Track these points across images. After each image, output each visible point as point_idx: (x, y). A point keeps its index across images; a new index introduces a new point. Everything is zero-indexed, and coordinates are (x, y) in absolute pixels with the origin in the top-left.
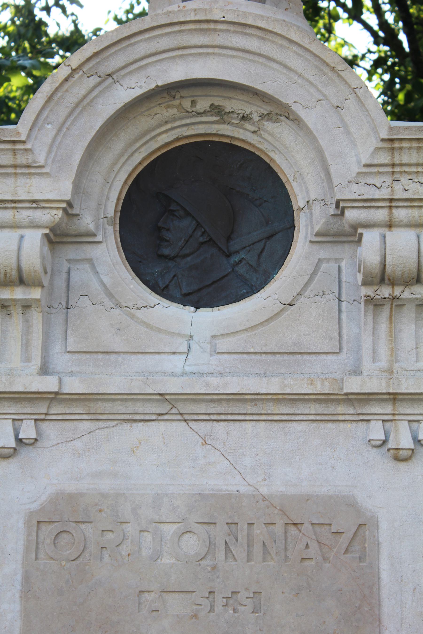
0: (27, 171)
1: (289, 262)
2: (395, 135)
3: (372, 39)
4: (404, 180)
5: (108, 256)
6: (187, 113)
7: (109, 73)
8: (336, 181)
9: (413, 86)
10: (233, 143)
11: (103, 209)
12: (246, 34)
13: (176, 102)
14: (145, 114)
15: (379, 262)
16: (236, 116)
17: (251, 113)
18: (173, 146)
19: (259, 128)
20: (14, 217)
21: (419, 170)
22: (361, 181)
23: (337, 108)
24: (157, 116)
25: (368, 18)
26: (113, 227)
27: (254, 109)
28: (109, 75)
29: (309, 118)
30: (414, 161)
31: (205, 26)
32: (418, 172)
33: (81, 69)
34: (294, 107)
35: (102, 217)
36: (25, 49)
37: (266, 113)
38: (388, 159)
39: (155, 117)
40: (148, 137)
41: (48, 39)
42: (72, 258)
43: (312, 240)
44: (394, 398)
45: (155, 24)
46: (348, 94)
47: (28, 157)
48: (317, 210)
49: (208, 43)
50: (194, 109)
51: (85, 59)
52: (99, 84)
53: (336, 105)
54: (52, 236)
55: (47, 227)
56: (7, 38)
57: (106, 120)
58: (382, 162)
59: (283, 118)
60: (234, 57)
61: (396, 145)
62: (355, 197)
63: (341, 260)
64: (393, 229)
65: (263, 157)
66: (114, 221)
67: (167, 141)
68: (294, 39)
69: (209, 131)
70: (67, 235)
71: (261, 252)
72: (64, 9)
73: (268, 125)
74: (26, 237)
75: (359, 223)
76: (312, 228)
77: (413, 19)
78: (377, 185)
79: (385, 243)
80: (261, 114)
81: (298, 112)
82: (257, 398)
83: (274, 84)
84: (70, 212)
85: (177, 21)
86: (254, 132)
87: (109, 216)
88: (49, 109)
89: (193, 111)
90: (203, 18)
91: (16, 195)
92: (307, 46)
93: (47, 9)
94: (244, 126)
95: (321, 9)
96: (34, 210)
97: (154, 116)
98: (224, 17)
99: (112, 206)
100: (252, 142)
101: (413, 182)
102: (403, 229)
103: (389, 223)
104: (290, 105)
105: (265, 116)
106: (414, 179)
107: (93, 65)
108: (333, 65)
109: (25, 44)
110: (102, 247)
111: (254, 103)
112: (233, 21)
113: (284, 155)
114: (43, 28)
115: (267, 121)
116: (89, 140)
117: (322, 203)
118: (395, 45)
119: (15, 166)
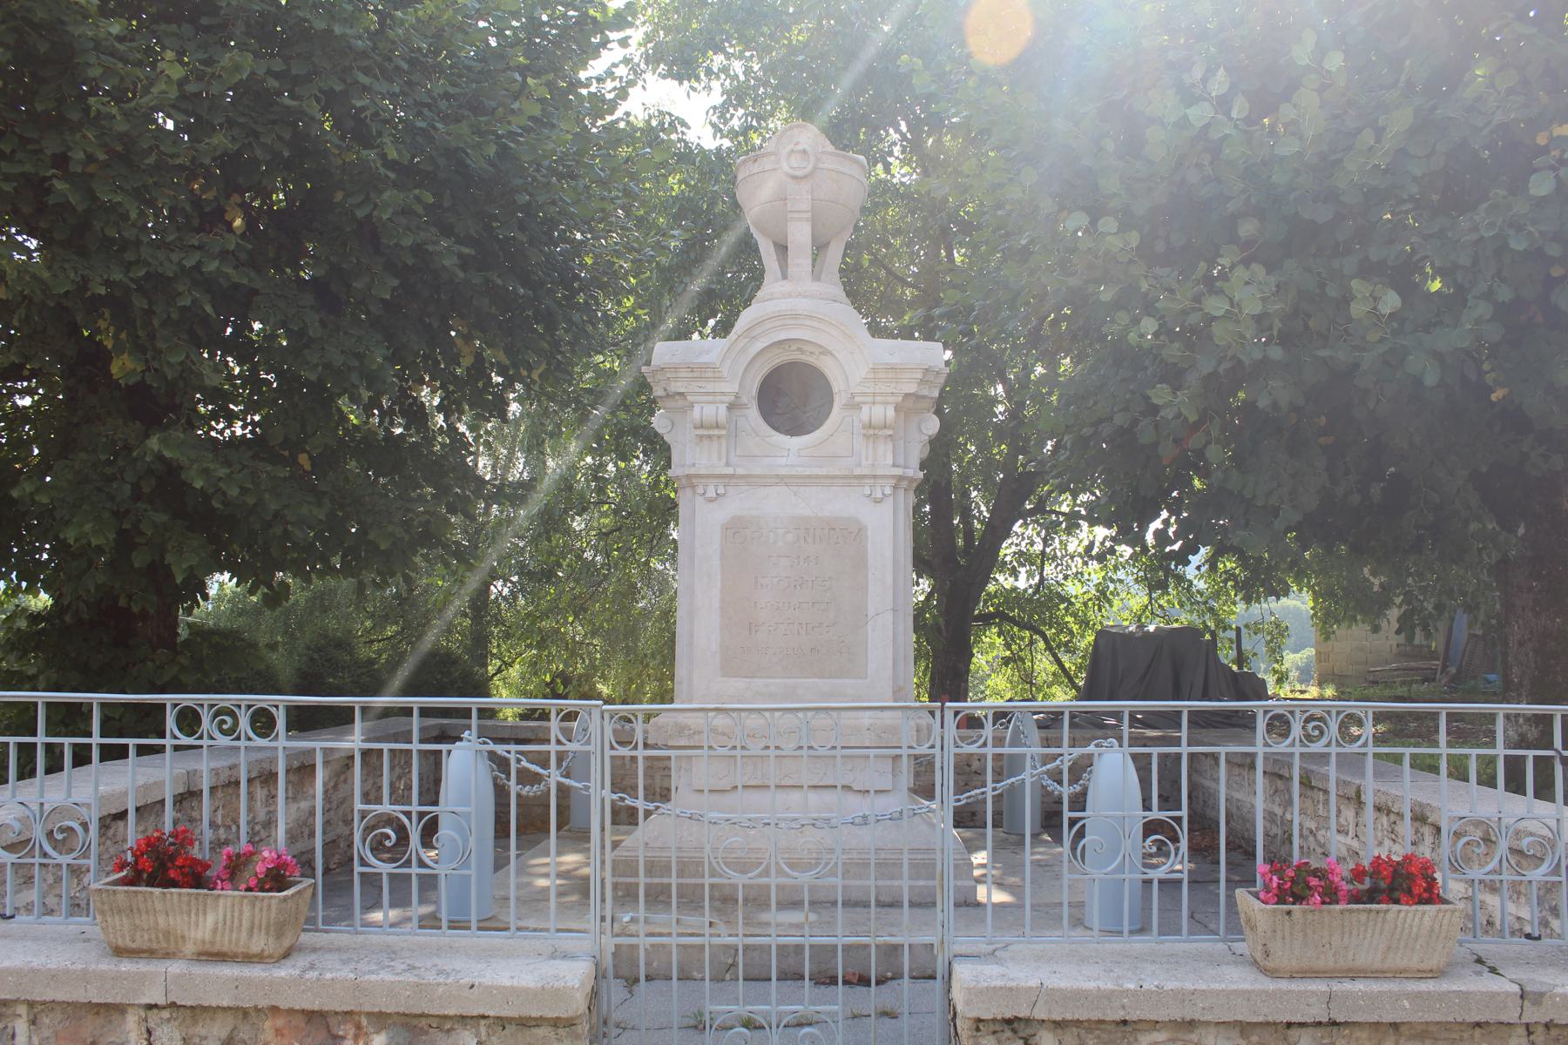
5: (753, 413)
44: (875, 477)
82: (817, 477)
99: (754, 392)
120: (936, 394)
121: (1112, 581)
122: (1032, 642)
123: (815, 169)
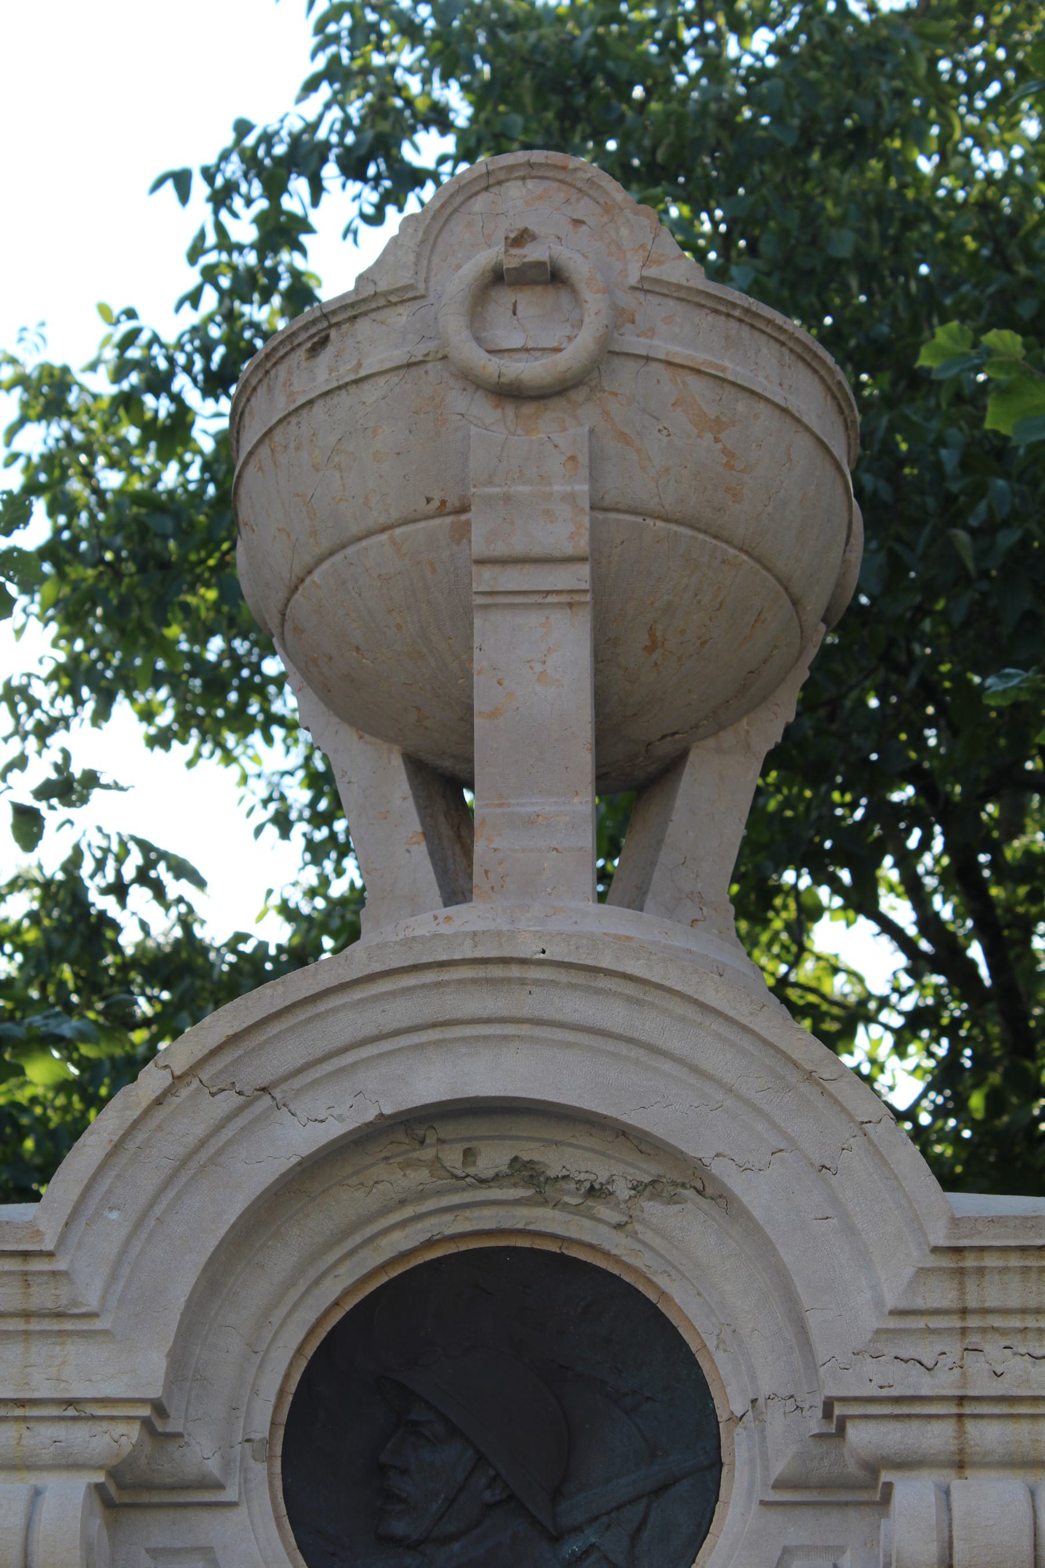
0: (56, 1328)
1: (709, 1555)
2: (966, 1237)
3: (901, 960)
4: (993, 1348)
6: (454, 1181)
7: (263, 1086)
8: (822, 1351)
9: (1006, 1076)
10: (566, 1252)
11: (242, 1420)
12: (598, 991)
13: (428, 1153)
14: (350, 1182)
15: (935, 1560)
16: (573, 1186)
17: (611, 1181)
18: (419, 1260)
19: (631, 1217)
20: (18, 1443)
21: (1029, 1325)
22: (885, 1352)
23: (820, 1171)
24: (380, 1187)
25: (894, 908)
26: (265, 1464)
27: (617, 1170)
28: (263, 1089)
29: (754, 1193)
30: (1014, 1301)
31: (497, 972)
32: (1026, 1328)
33: (194, 1076)
34: (717, 1168)
35: (240, 1440)
36: (62, 984)
37: (647, 1179)
38: (950, 1296)
39: (374, 1190)
40: (357, 1239)
41: (118, 959)
42: (161, 1546)
43: (766, 1499)
45: (377, 967)
46: (847, 1136)
47: (58, 1292)
48: (776, 1422)
49: (505, 1013)
50: (471, 1171)
51: (206, 1051)
52: (240, 1110)
53: (818, 1163)
54: (112, 1489)
55: (100, 1468)
56: (19, 957)
57: (253, 1198)
58: (935, 1305)
59: (689, 1193)
60: (568, 1045)
61: (970, 1262)
62: (872, 1391)
63: (841, 1550)
64: (968, 1472)
65: (641, 1289)
66: (270, 1449)
67: (403, 1249)
68: (713, 1004)
69: (507, 1225)
70: (150, 1487)
71: (639, 1529)
72: (158, 890)
73: (653, 1209)
74: (47, 1494)
75: (883, 1458)
76: (766, 1468)
77: (999, 912)
78: (924, 1362)
79: (949, 1509)
80: (635, 1183)
81: (725, 1180)
83: (666, 1110)
84: (160, 1429)
85: (430, 960)
86: (619, 1226)
87: (256, 1436)
88: (114, 1173)
89: (468, 1176)
90: (494, 954)
91: (26, 1387)
92: (745, 1021)
93: (119, 890)
94: (595, 1211)
95: (778, 889)
96: (70, 1424)
97: (372, 1187)
98: (544, 952)
100: (614, 1251)
101: (1015, 1354)
102: (993, 1474)
103: (957, 1458)
104: (705, 1161)
105: (646, 1186)
106: (1017, 1347)
107: (226, 1066)
108: (808, 1067)
109: (62, 972)
110: (239, 1515)
111: (617, 1155)
112: (566, 960)
113: (693, 1286)
114: (109, 934)
115: (649, 1200)
116: (212, 1249)
117: (790, 1405)
118: (961, 972)
119: (27, 1315)
123: (608, 353)
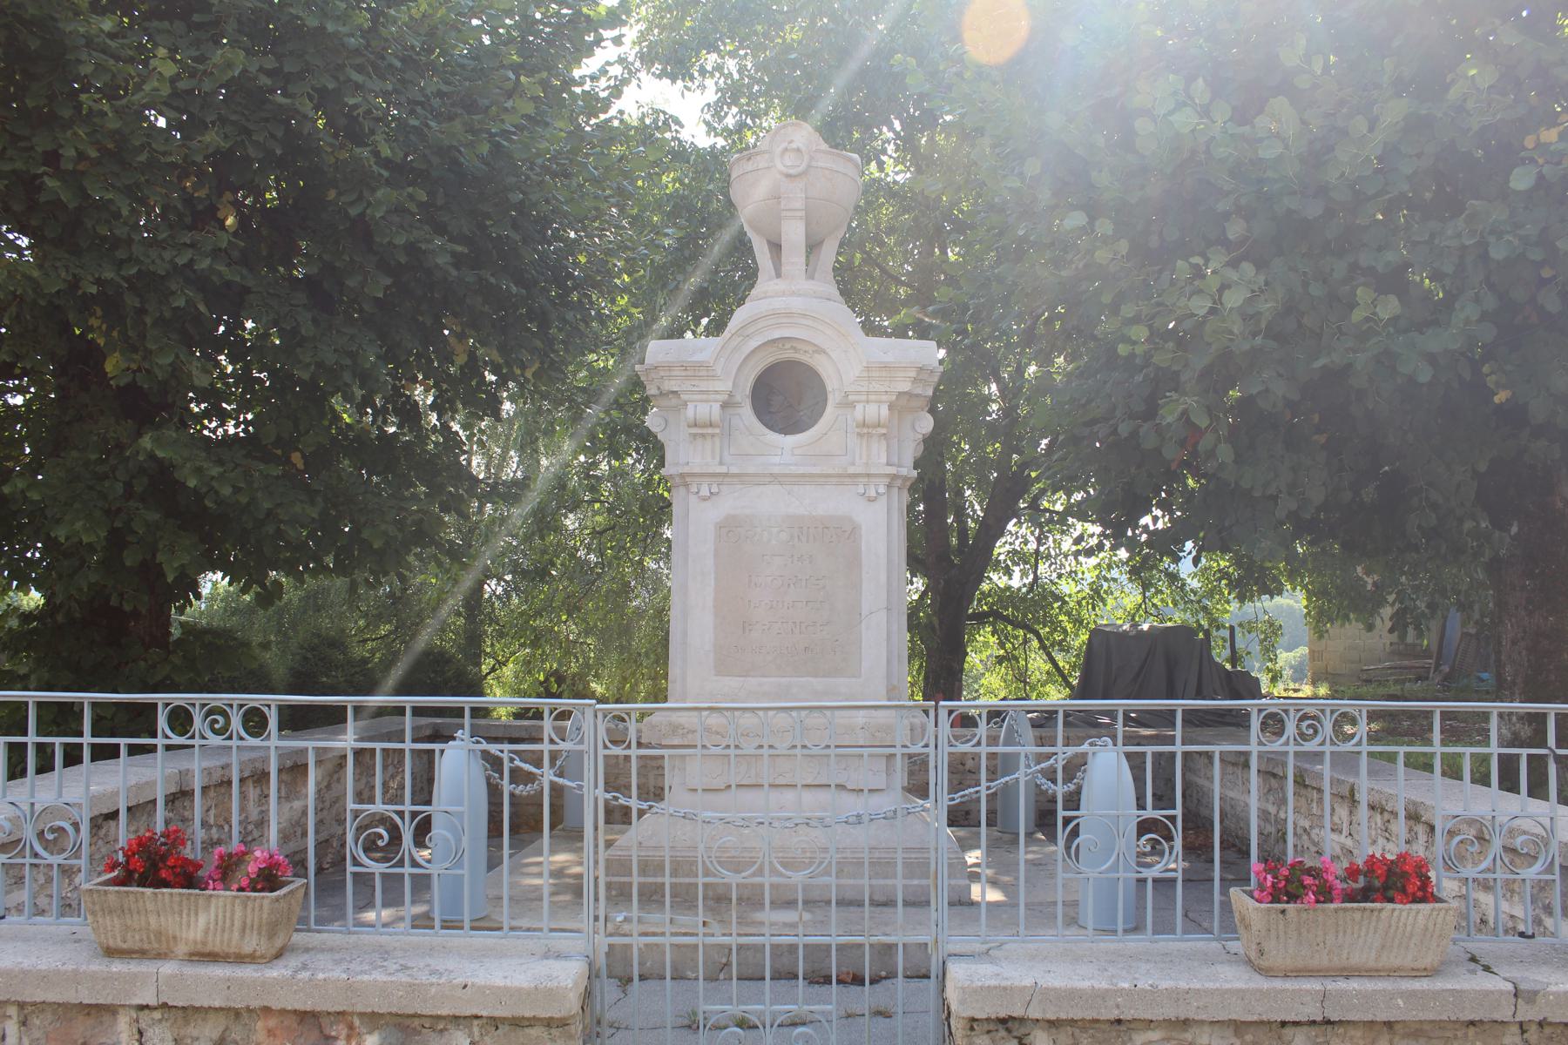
5: (747, 412)
44: (868, 475)
82: (811, 475)
120: (930, 392)
121: (1106, 579)
122: (1026, 641)
123: (809, 166)
